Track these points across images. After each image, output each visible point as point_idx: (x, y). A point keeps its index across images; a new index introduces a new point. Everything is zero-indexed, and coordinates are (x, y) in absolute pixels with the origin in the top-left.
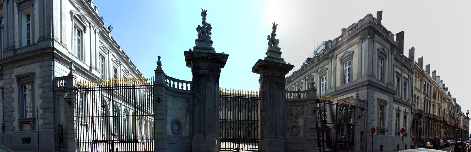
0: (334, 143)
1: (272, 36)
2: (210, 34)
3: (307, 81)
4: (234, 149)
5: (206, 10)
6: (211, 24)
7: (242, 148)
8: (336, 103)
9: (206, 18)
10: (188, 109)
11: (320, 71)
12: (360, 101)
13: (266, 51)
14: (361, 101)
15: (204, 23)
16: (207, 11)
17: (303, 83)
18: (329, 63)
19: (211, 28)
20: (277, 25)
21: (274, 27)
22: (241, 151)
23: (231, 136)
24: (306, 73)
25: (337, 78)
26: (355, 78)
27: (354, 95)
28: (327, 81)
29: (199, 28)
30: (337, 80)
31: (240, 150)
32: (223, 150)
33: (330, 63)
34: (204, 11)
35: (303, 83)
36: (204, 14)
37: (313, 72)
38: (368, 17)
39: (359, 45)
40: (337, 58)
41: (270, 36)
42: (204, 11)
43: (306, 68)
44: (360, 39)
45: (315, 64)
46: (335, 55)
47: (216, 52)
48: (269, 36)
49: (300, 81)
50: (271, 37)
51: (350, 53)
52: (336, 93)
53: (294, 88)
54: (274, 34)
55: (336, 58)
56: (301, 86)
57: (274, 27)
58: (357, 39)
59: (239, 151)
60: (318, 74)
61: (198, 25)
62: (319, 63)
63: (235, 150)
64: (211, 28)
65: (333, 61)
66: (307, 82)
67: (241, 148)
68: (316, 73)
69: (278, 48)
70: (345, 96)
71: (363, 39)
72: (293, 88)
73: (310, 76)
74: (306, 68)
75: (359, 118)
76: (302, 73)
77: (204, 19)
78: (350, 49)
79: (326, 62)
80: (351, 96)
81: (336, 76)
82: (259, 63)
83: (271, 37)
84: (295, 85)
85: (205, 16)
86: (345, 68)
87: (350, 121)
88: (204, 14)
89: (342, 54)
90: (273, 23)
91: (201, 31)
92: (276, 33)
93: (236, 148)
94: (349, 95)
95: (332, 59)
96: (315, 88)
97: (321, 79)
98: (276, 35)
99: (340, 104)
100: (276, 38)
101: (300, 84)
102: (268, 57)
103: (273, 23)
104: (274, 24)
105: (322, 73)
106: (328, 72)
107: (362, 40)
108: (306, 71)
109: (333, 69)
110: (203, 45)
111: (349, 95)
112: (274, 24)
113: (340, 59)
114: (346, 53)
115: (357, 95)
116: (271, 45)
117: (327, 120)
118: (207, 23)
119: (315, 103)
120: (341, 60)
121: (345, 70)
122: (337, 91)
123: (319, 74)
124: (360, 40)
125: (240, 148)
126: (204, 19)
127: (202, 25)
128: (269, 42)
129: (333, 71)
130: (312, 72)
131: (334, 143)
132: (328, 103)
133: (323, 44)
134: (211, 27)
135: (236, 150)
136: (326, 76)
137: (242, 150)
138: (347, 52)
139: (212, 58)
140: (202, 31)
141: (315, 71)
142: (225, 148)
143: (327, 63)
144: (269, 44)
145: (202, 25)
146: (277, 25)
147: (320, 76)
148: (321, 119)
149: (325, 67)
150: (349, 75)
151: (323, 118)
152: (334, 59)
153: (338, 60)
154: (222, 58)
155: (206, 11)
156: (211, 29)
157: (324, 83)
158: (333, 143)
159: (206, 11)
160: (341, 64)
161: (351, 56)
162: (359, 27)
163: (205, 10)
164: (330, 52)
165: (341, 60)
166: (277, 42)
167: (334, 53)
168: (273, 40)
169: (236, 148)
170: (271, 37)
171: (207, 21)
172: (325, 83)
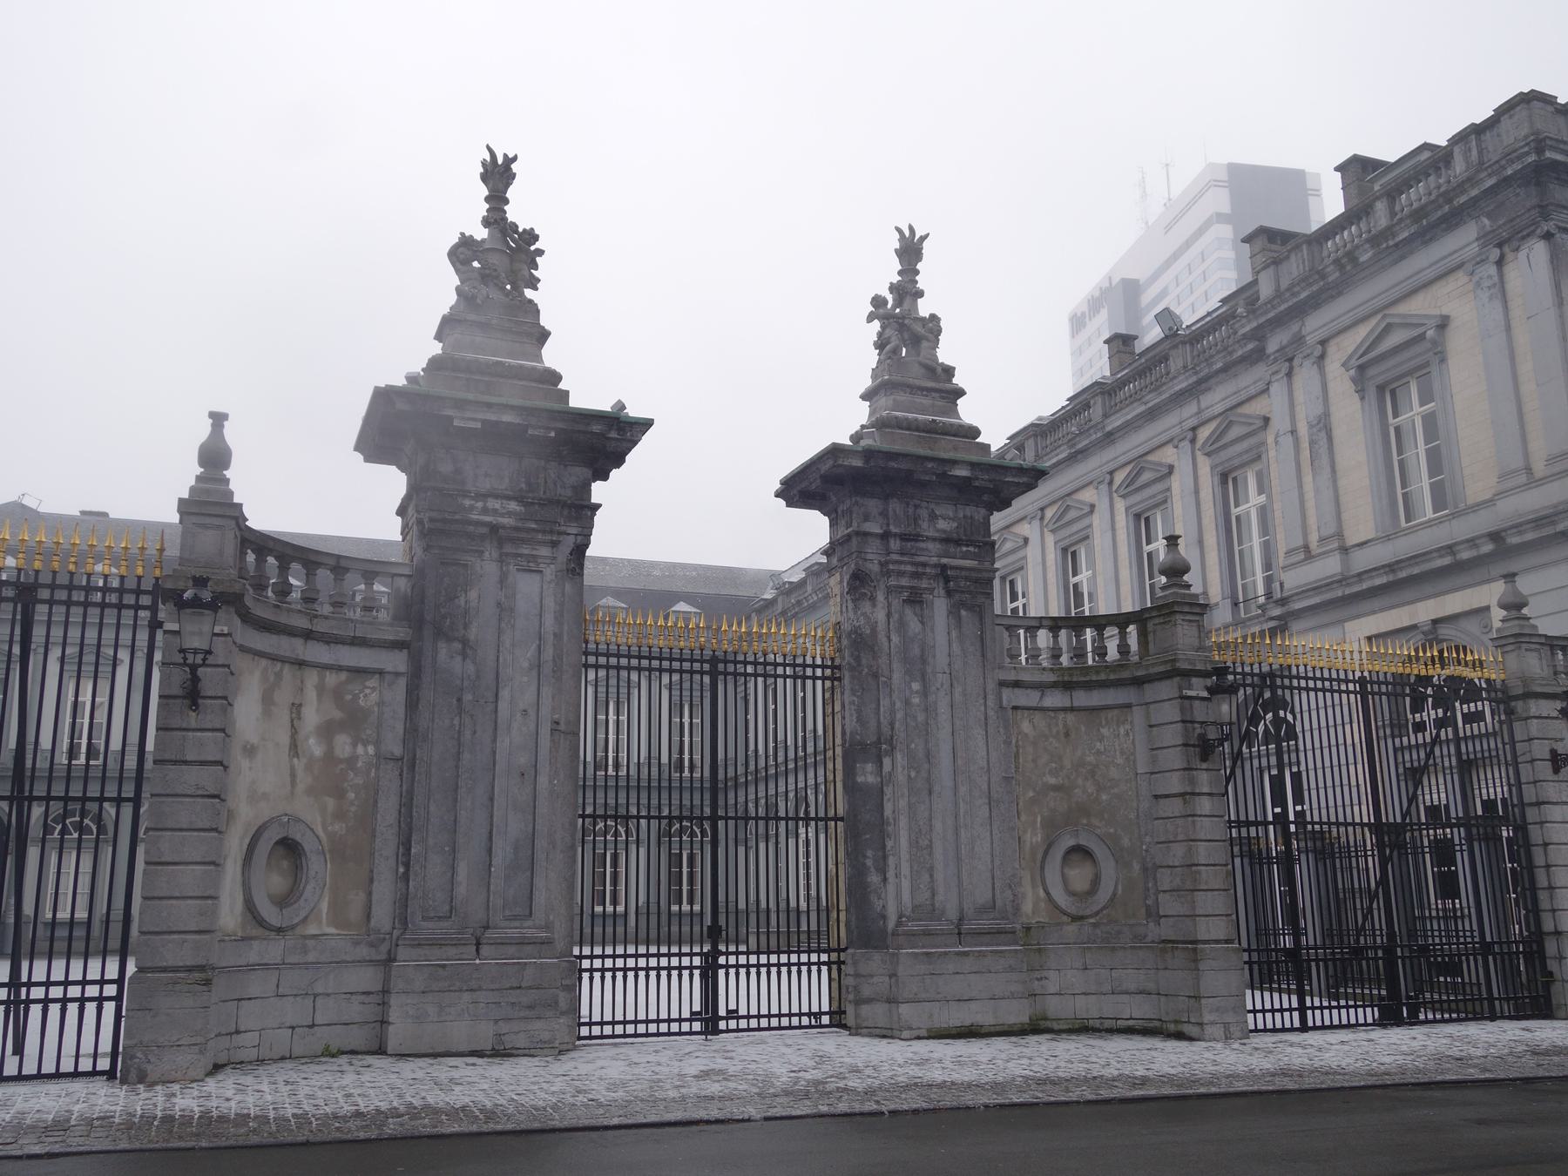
0: (1376, 959)
1: (899, 302)
2: (533, 283)
3: (1124, 496)
4: (686, 1014)
5: (510, 156)
6: (537, 232)
7: (732, 1006)
8: (1354, 682)
9: (511, 193)
10: (21, 555)
11: (1131, 481)
12: (1546, 650)
13: (866, 382)
14: (1552, 647)
15: (496, 217)
16: (515, 159)
17: (1092, 512)
18: (1274, 388)
19: (540, 252)
20: (927, 235)
21: (910, 250)
22: (728, 1031)
23: (615, 894)
24: (1113, 442)
25: (1342, 483)
26: (1477, 480)
27: (1490, 594)
28: (1270, 497)
29: (463, 252)
30: (1343, 499)
31: (722, 1025)
32: (653, 1028)
33: (1278, 389)
34: (500, 161)
35: (1093, 506)
36: (498, 175)
37: (1164, 438)
38: (1521, 112)
39: (1476, 278)
40: (1328, 361)
41: (885, 302)
42: (500, 161)
43: (1106, 416)
44: (1484, 239)
45: (1177, 388)
46: (1311, 340)
47: (574, 402)
48: (878, 302)
49: (1069, 495)
50: (889, 306)
51: (1420, 330)
52: (1348, 591)
53: (1026, 540)
54: (907, 290)
55: (1322, 357)
56: (1076, 527)
57: (910, 250)
58: (1464, 239)
59: (717, 1031)
60: (1198, 453)
61: (463, 234)
62: (1199, 382)
63: (690, 1020)
64: (540, 252)
65: (1298, 381)
66: (1120, 505)
67: (728, 1012)
68: (1104, 487)
69: (939, 370)
70: (1421, 605)
71: (1504, 244)
72: (1021, 542)
73: (1139, 463)
74: (1106, 416)
75: (1556, 770)
76: (1079, 446)
77: (497, 199)
78: (1417, 306)
79: (1248, 379)
80: (1467, 608)
81: (1334, 470)
82: (831, 462)
83: (889, 306)
84: (1036, 523)
85: (1184, 1034)
86: (1237, 505)
87: (1492, 786)
88: (498, 175)
89: (1362, 332)
90: (898, 230)
91: (476, 264)
92: (922, 282)
93: (697, 1008)
94: (1454, 603)
95: (1290, 360)
96: (1196, 596)
97: (1070, 557)
98: (920, 294)
99: (1387, 684)
100: (924, 308)
101: (1072, 514)
102: (880, 424)
103: (898, 230)
104: (907, 234)
105: (1225, 447)
106: (1270, 439)
107: (1500, 245)
108: (1110, 434)
109: (1311, 426)
110: (495, 352)
111: (1454, 603)
112: (907, 234)
113: (1354, 363)
114: (1388, 329)
115: (1515, 606)
116: (896, 351)
117: (1299, 772)
118: (517, 226)
119: (1205, 694)
120: (1361, 372)
121: (1238, 518)
122: (1360, 575)
123: (1208, 454)
124: (1484, 246)
125: (722, 1012)
126: (497, 199)
127: (481, 233)
128: (880, 335)
129: (1312, 443)
130: (1156, 442)
131: (1376, 959)
132: (1295, 683)
133: (1216, 183)
134: (538, 245)
135: (697, 1026)
136: (1257, 467)
137: (733, 1024)
138: (1397, 320)
139: (553, 434)
140: (483, 268)
141: (1177, 430)
142: (664, 1016)
143: (1261, 386)
144: (880, 345)
145: (481, 233)
146: (923, 238)
147: (1127, 510)
148: (1256, 762)
149: (1247, 409)
150: (1435, 462)
151: (1273, 760)
152: (1307, 363)
153: (1334, 366)
154: (613, 434)
155: (509, 161)
156: (538, 259)
157: (1248, 513)
158: (1368, 959)
159: (509, 161)
160: (1362, 398)
161: (1426, 345)
162: (1459, 166)
163: (505, 155)
164: (1278, 322)
165: (1362, 368)
166: (931, 331)
167: (1303, 324)
168: (906, 321)
169: (697, 1008)
170: (894, 307)
171: (519, 212)
172: (1263, 511)
